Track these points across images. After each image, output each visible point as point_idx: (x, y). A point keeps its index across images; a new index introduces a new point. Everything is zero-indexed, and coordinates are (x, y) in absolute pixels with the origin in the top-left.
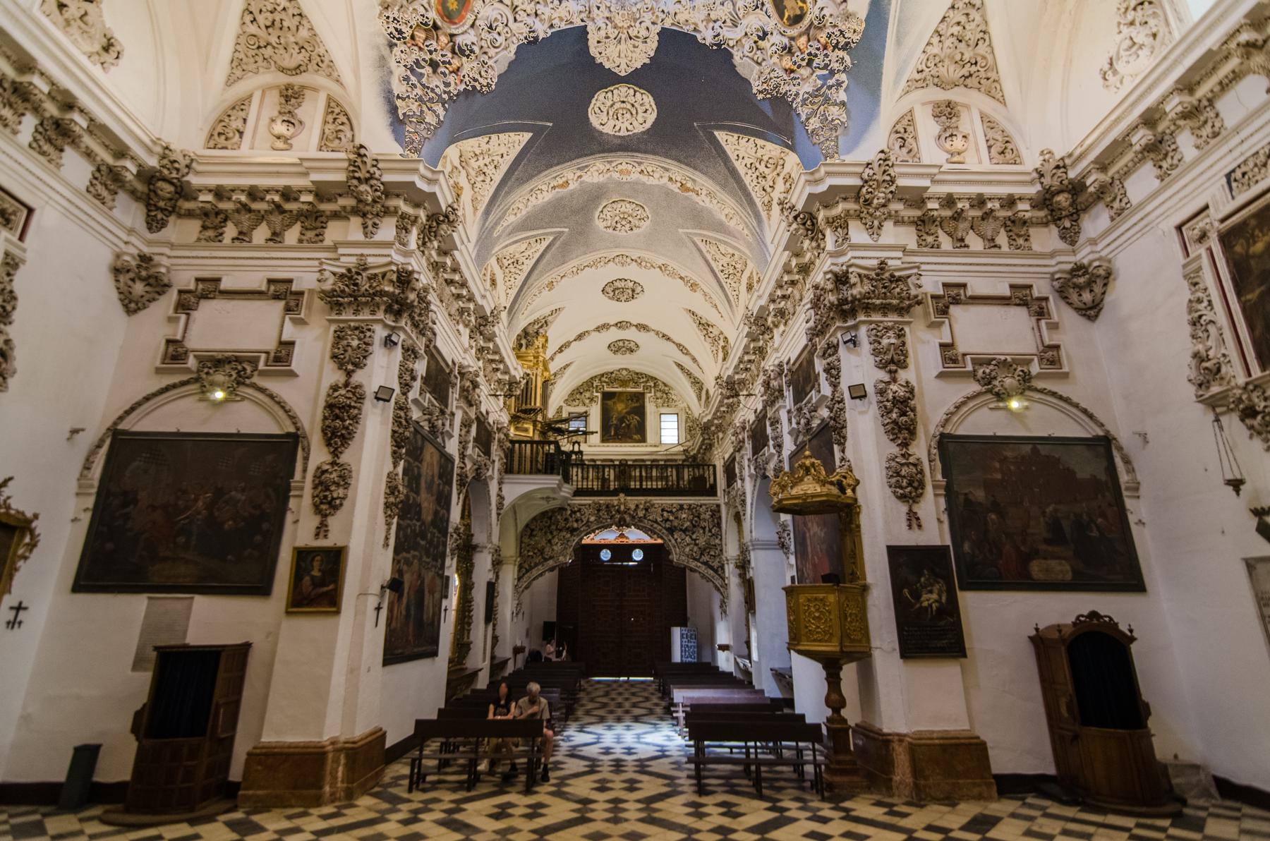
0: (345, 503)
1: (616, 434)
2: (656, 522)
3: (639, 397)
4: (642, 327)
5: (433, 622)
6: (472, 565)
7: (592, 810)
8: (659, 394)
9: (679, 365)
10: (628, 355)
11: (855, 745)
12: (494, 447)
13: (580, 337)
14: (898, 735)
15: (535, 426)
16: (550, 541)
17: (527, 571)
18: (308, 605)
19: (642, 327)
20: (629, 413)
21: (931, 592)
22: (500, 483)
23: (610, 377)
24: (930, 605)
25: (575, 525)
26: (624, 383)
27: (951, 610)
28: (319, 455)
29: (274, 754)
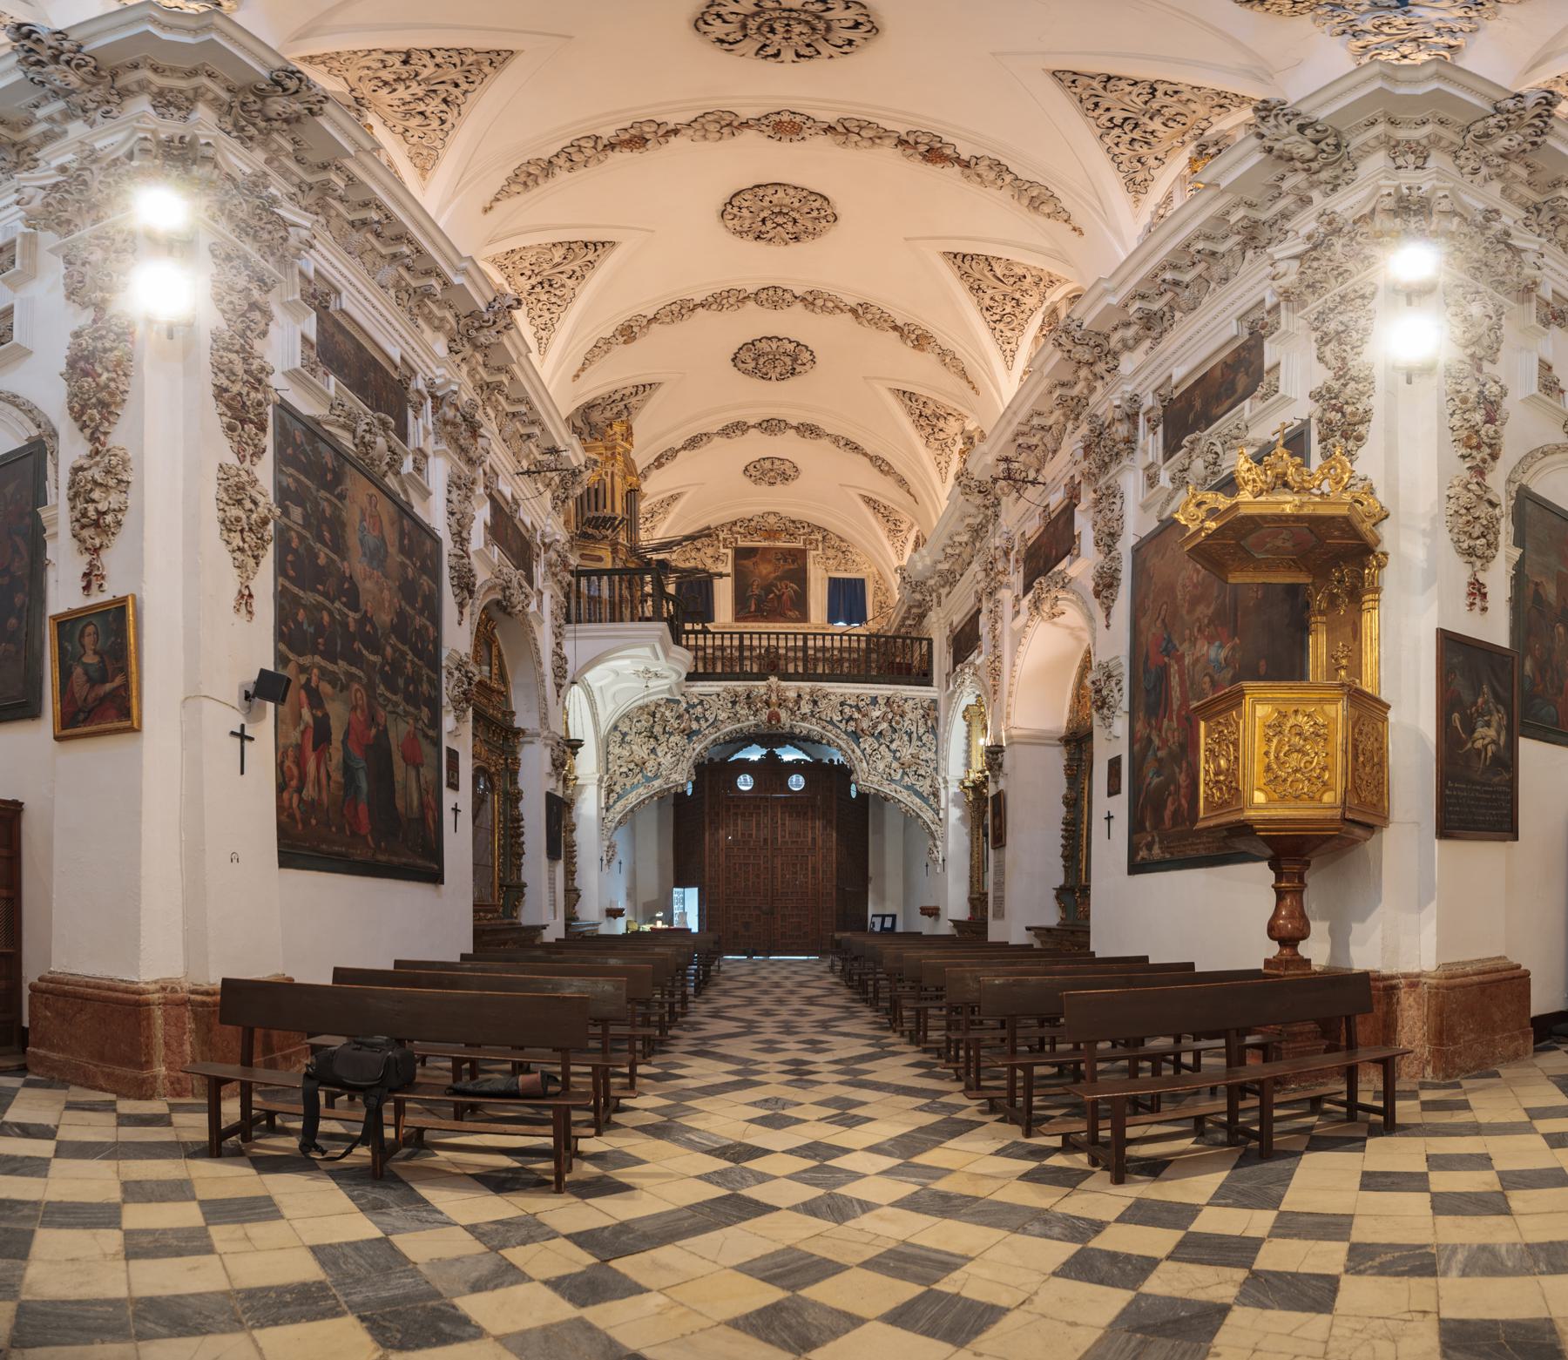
0: (125, 519)
1: (759, 609)
2: (831, 722)
3: (799, 556)
4: (809, 430)
5: (423, 819)
6: (516, 761)
7: (762, 1178)
8: (831, 553)
9: (868, 501)
10: (779, 487)
11: (787, 689)
12: (539, 570)
13: (693, 443)
14: (1405, 976)
15: (615, 551)
16: (653, 751)
17: (620, 797)
18: (85, 722)
19: (809, 430)
20: (780, 578)
21: (1488, 724)
22: (558, 635)
23: (748, 526)
24: (1485, 747)
25: (695, 726)
26: (771, 534)
27: (1507, 763)
28: (71, 449)
29: (65, 994)
